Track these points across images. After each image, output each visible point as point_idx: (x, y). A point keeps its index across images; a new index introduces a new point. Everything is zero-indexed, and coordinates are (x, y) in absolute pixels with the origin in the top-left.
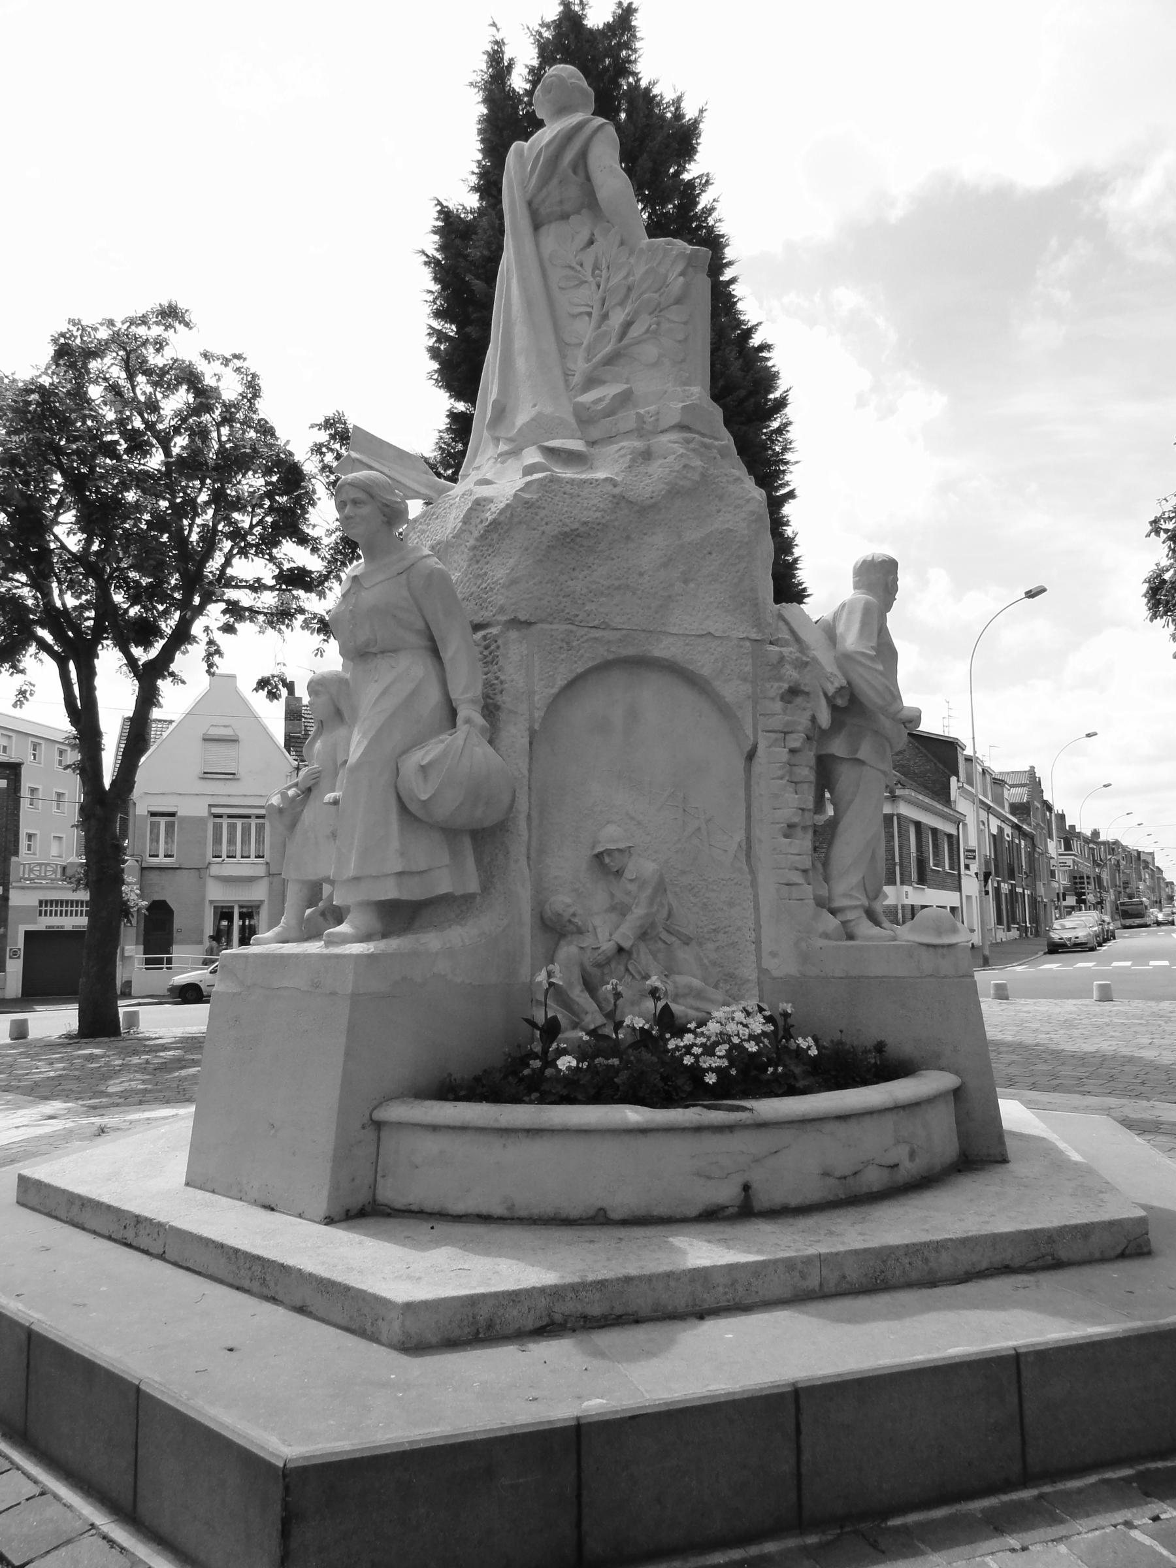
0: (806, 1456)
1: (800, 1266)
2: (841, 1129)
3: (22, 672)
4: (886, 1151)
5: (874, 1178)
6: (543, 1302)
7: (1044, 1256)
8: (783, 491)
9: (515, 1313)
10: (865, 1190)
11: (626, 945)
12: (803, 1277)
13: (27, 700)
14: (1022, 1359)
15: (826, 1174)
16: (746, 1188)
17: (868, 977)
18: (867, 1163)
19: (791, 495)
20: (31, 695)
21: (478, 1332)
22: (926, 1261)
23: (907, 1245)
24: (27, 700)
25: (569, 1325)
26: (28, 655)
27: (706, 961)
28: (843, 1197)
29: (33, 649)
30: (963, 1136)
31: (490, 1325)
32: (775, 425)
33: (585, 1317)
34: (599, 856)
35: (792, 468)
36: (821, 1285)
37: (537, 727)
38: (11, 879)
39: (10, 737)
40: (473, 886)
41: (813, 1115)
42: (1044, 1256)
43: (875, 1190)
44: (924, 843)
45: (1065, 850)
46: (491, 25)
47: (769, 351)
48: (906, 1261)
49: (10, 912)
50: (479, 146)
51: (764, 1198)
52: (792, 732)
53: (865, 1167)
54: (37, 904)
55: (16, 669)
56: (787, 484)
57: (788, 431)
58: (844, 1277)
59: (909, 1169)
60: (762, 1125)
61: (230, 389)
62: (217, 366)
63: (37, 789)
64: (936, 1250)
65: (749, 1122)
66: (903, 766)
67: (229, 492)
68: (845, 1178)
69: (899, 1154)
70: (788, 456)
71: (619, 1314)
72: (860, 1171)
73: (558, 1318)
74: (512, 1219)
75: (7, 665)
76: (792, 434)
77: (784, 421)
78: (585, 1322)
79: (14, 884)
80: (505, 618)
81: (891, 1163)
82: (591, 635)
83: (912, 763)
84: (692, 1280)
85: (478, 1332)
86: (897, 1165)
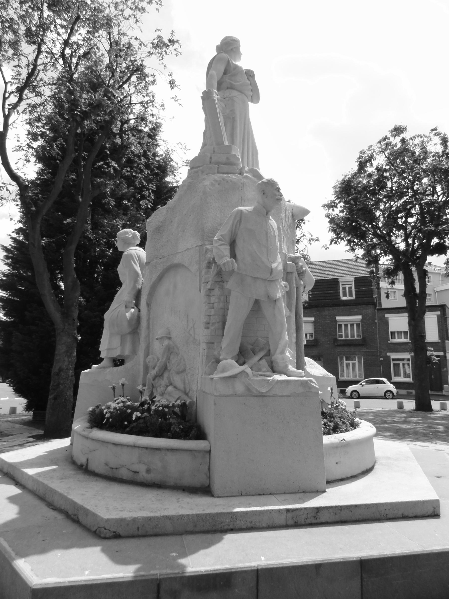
4: (132, 464)
5: (124, 473)
10: (120, 477)
15: (106, 464)
18: (123, 466)
28: (111, 476)
41: (106, 441)
45: (399, 365)
50: (219, 43)
52: (209, 282)
53: (122, 467)
59: (143, 476)
63: (431, 294)
67: (114, 203)
68: (113, 468)
69: (142, 468)
80: (387, 189)
81: (135, 470)
86: (138, 472)
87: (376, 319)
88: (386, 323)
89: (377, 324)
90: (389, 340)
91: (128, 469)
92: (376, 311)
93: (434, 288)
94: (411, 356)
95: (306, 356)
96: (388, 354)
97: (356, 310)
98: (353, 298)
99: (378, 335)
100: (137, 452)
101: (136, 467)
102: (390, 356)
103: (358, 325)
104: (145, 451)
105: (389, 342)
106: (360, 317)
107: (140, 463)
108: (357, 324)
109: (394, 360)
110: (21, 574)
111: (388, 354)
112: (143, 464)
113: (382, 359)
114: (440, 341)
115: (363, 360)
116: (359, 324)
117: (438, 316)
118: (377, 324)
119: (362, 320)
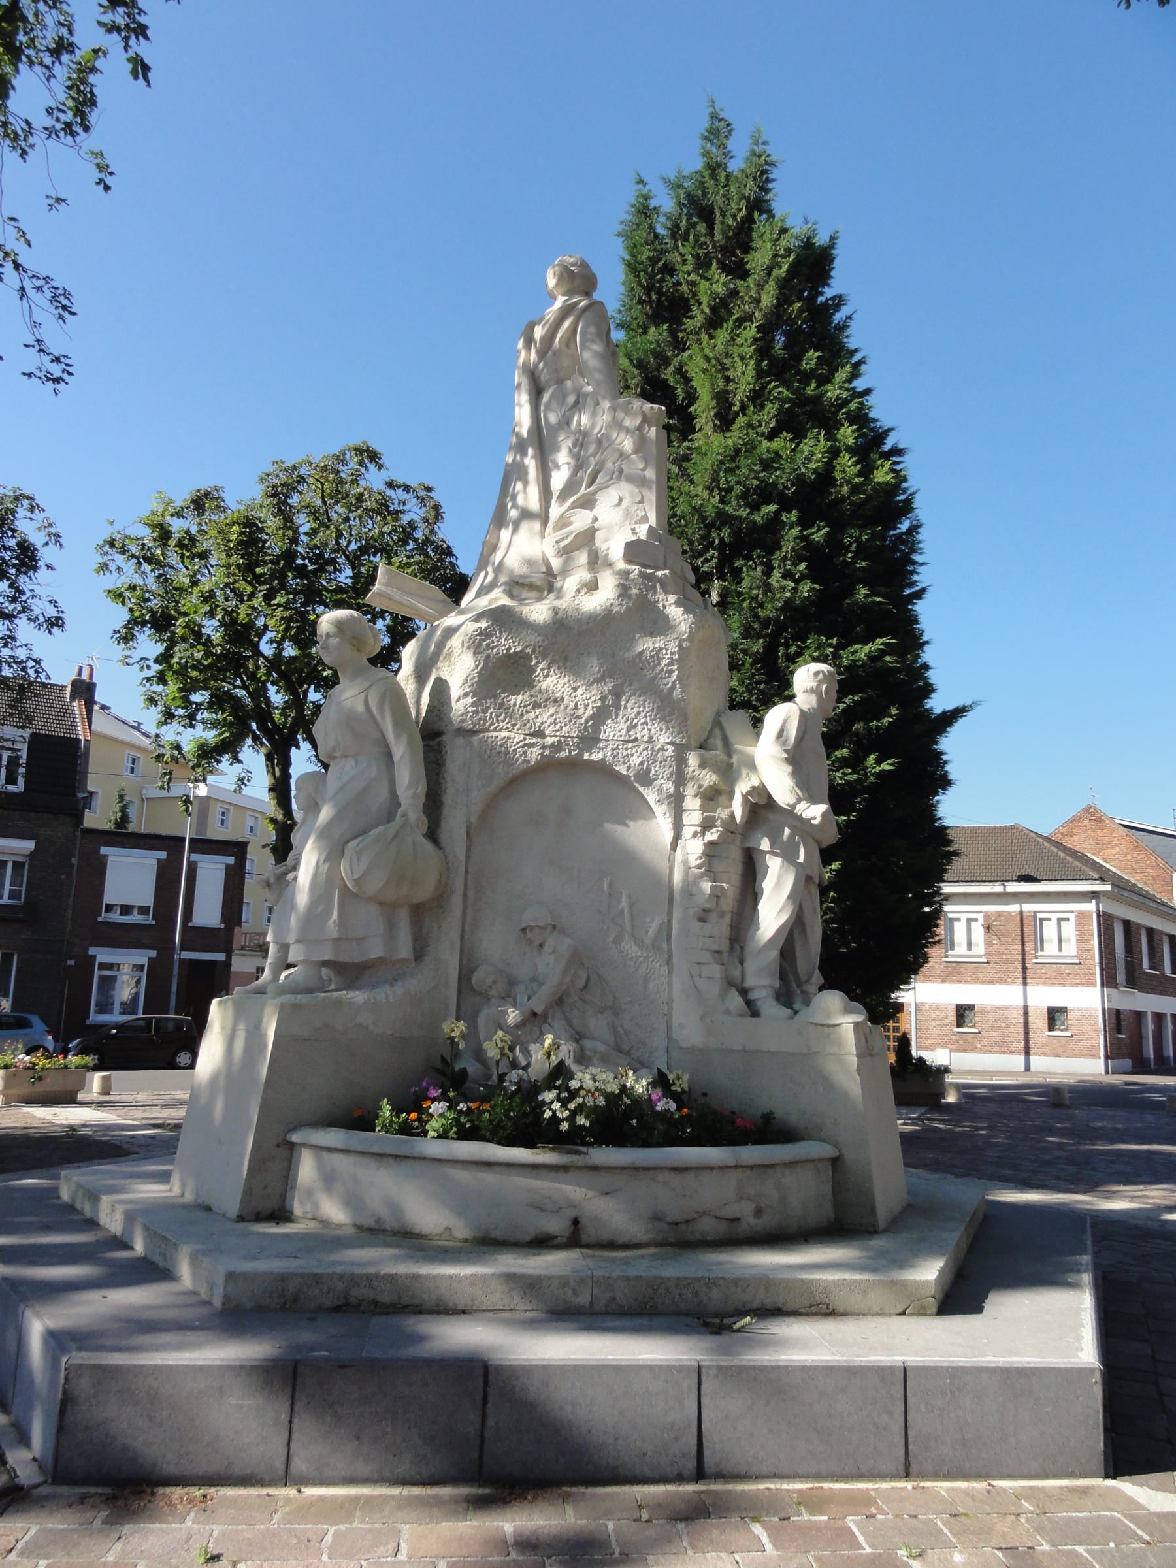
0: (491, 1422)
1: (572, 1284)
2: (676, 1180)
3: (240, 762)
6: (340, 1286)
7: (818, 1305)
8: (908, 592)
9: (317, 1291)
10: (699, 1237)
11: (539, 1010)
12: (575, 1293)
13: (246, 785)
14: (704, 1371)
16: (576, 1222)
17: (762, 1052)
18: (702, 1214)
19: (919, 595)
20: (248, 781)
21: (285, 1304)
22: (696, 1294)
23: (678, 1278)
24: (246, 785)
25: (362, 1308)
26: (246, 745)
27: (620, 1029)
29: (249, 741)
30: (839, 1204)
31: (295, 1299)
32: (904, 526)
33: (376, 1303)
34: (524, 930)
35: (920, 569)
36: (591, 1303)
37: (473, 819)
38: (234, 946)
39: (256, 818)
40: (404, 949)
42: (818, 1305)
43: (709, 1238)
44: (1133, 944)
46: (638, 183)
47: (900, 456)
48: (676, 1292)
49: (232, 976)
51: (590, 1232)
54: (255, 970)
55: (236, 760)
56: (914, 583)
57: (918, 533)
58: (614, 1299)
59: (750, 1223)
60: (595, 1168)
61: (414, 512)
62: (401, 494)
64: (707, 1285)
65: (579, 1164)
66: (1121, 861)
68: (676, 1224)
69: (745, 1210)
70: (917, 558)
71: (405, 1304)
72: (694, 1220)
73: (352, 1300)
74: (378, 1230)
75: (227, 756)
76: (923, 535)
77: (914, 523)
78: (376, 1307)
79: (236, 952)
82: (527, 742)
83: (1129, 856)
84: (473, 1284)
85: (285, 1304)
86: (738, 1219)
87: (74, 856)
88: (99, 868)
89: (75, 868)
90: (100, 915)
91: (717, 1217)
92: (79, 833)
93: (143, 788)
94: (150, 959)
95: (830, 983)
96: (92, 951)
97: (21, 823)
98: (20, 786)
99: (72, 899)
100: (733, 1177)
101: (732, 1210)
102: (94, 957)
103: (18, 866)
104: (748, 1172)
105: (100, 919)
106: (29, 845)
107: (742, 1198)
108: (15, 863)
109: (102, 966)
110: (1098, 1347)
111: (92, 951)
112: (748, 1199)
113: (71, 962)
114: (223, 926)
115: (18, 963)
116: (23, 864)
117: (228, 867)
118: (75, 868)
119: (32, 855)
